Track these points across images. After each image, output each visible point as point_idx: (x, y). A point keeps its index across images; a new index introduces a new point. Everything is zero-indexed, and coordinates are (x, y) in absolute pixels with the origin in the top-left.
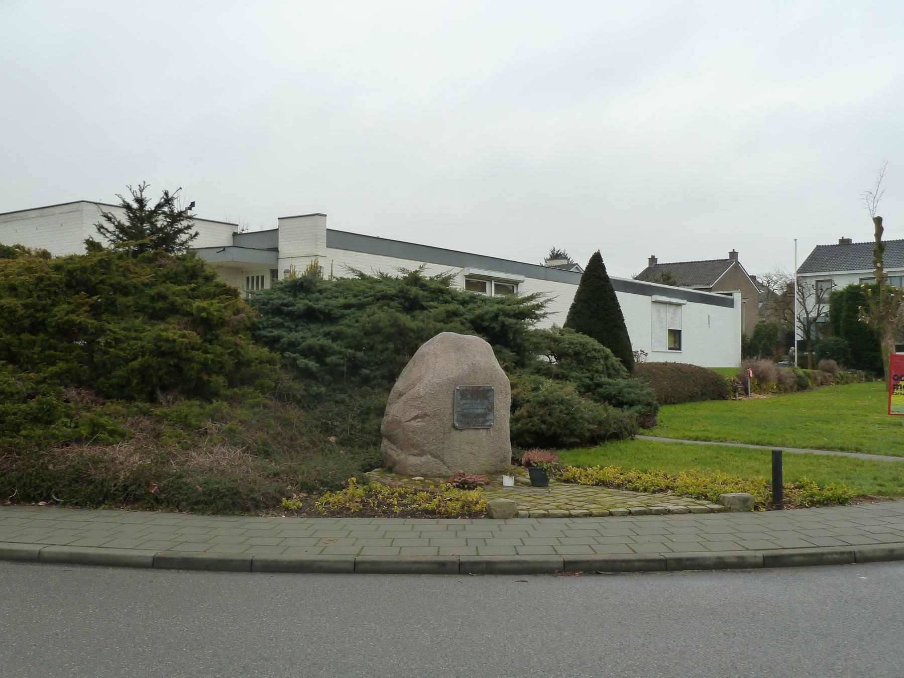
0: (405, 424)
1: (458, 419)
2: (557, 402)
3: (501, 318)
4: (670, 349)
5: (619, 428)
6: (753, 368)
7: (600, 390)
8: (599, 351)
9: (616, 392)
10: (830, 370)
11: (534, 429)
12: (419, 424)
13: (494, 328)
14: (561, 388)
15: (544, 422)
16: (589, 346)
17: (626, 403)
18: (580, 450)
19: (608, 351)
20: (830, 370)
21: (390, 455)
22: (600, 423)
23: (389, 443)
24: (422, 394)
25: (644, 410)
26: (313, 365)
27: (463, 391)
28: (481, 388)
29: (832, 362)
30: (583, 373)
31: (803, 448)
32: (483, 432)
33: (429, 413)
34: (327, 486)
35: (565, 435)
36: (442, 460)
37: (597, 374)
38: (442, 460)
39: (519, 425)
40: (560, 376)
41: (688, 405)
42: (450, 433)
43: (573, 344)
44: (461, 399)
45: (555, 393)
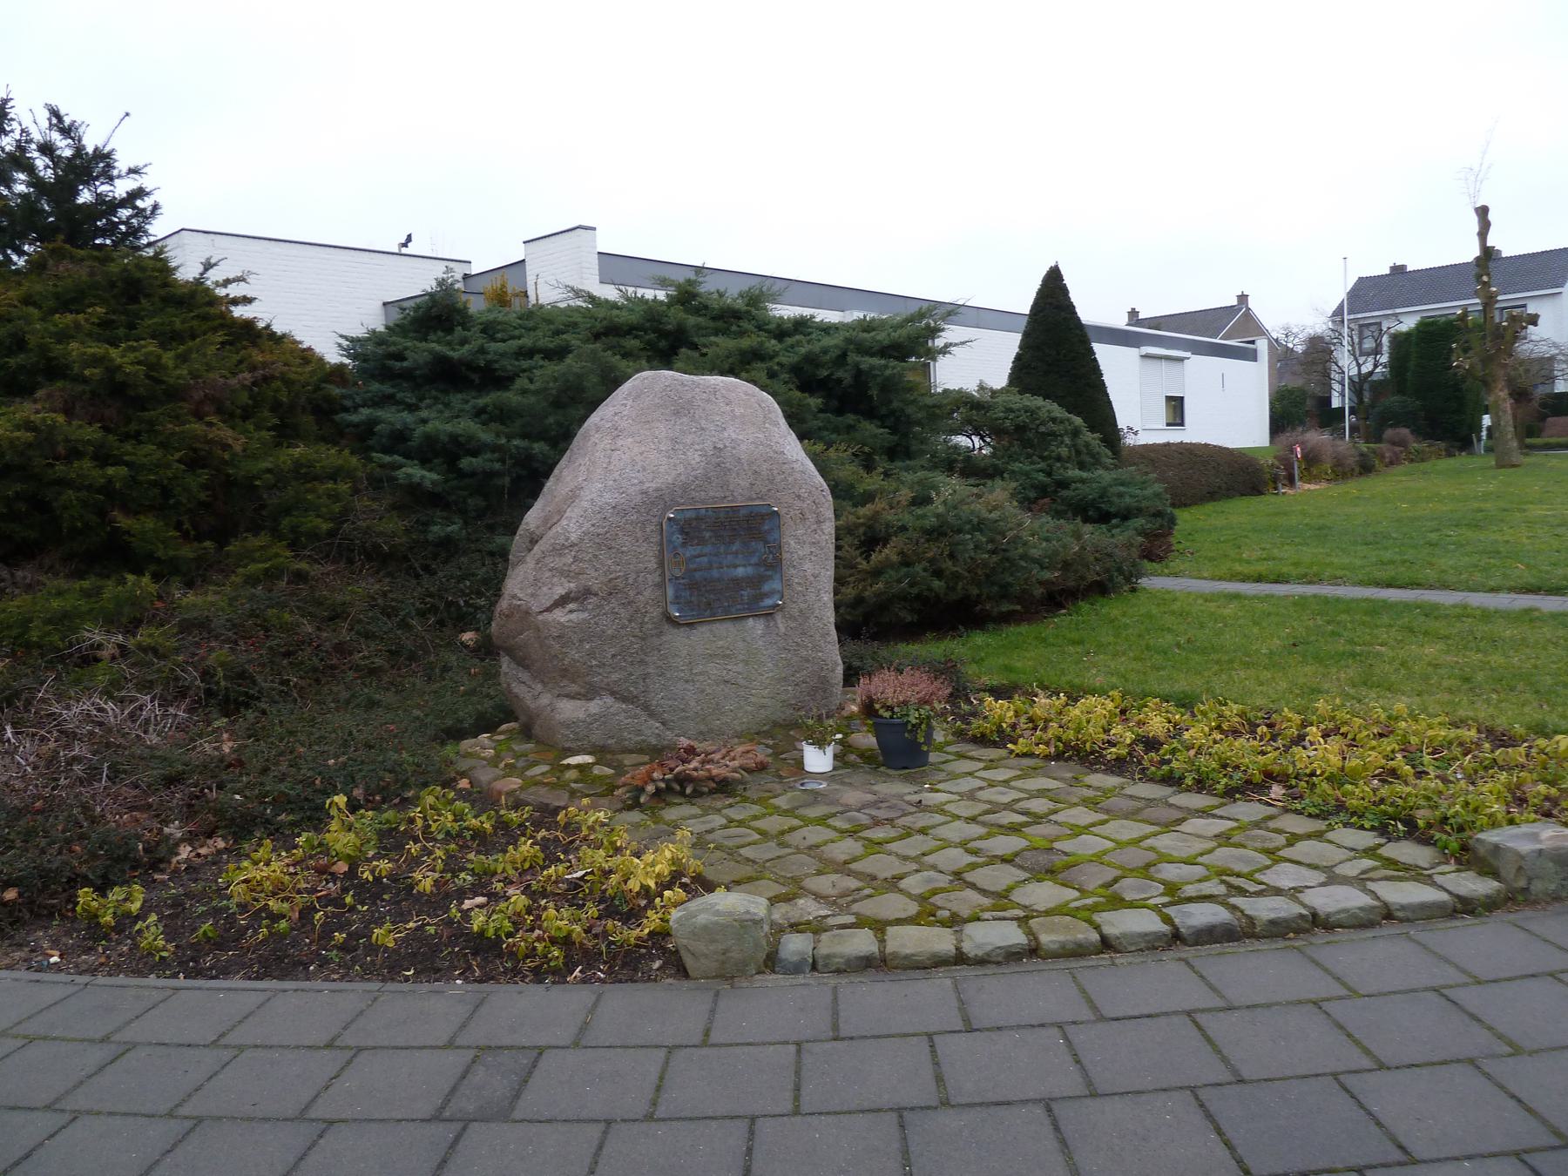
0: (540, 617)
1: (677, 597)
2: (968, 527)
3: (853, 358)
4: (1168, 425)
5: (1107, 570)
6: (1302, 444)
7: (1065, 493)
8: (1062, 422)
9: (1096, 495)
10: (1402, 443)
11: (915, 591)
12: (573, 616)
13: (840, 381)
14: (979, 496)
15: (938, 574)
16: (1043, 414)
17: (1115, 516)
18: (1024, 628)
19: (1078, 421)
20: (1402, 443)
21: (517, 697)
22: (1066, 566)
23: (513, 665)
24: (574, 537)
25: (1149, 526)
26: (427, 477)
27: (688, 522)
28: (743, 512)
29: (1405, 432)
30: (1032, 463)
31: (1492, 590)
32: (756, 627)
33: (595, 588)
34: (302, 808)
35: (989, 598)
36: (645, 707)
37: (1058, 465)
38: (645, 707)
39: (880, 585)
40: (990, 471)
41: (1209, 507)
42: (660, 634)
43: (1011, 410)
44: (684, 544)
45: (965, 507)
